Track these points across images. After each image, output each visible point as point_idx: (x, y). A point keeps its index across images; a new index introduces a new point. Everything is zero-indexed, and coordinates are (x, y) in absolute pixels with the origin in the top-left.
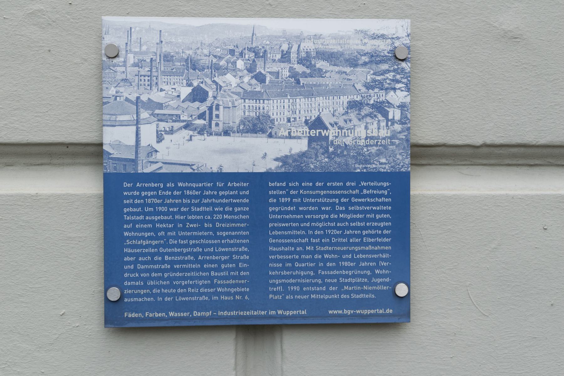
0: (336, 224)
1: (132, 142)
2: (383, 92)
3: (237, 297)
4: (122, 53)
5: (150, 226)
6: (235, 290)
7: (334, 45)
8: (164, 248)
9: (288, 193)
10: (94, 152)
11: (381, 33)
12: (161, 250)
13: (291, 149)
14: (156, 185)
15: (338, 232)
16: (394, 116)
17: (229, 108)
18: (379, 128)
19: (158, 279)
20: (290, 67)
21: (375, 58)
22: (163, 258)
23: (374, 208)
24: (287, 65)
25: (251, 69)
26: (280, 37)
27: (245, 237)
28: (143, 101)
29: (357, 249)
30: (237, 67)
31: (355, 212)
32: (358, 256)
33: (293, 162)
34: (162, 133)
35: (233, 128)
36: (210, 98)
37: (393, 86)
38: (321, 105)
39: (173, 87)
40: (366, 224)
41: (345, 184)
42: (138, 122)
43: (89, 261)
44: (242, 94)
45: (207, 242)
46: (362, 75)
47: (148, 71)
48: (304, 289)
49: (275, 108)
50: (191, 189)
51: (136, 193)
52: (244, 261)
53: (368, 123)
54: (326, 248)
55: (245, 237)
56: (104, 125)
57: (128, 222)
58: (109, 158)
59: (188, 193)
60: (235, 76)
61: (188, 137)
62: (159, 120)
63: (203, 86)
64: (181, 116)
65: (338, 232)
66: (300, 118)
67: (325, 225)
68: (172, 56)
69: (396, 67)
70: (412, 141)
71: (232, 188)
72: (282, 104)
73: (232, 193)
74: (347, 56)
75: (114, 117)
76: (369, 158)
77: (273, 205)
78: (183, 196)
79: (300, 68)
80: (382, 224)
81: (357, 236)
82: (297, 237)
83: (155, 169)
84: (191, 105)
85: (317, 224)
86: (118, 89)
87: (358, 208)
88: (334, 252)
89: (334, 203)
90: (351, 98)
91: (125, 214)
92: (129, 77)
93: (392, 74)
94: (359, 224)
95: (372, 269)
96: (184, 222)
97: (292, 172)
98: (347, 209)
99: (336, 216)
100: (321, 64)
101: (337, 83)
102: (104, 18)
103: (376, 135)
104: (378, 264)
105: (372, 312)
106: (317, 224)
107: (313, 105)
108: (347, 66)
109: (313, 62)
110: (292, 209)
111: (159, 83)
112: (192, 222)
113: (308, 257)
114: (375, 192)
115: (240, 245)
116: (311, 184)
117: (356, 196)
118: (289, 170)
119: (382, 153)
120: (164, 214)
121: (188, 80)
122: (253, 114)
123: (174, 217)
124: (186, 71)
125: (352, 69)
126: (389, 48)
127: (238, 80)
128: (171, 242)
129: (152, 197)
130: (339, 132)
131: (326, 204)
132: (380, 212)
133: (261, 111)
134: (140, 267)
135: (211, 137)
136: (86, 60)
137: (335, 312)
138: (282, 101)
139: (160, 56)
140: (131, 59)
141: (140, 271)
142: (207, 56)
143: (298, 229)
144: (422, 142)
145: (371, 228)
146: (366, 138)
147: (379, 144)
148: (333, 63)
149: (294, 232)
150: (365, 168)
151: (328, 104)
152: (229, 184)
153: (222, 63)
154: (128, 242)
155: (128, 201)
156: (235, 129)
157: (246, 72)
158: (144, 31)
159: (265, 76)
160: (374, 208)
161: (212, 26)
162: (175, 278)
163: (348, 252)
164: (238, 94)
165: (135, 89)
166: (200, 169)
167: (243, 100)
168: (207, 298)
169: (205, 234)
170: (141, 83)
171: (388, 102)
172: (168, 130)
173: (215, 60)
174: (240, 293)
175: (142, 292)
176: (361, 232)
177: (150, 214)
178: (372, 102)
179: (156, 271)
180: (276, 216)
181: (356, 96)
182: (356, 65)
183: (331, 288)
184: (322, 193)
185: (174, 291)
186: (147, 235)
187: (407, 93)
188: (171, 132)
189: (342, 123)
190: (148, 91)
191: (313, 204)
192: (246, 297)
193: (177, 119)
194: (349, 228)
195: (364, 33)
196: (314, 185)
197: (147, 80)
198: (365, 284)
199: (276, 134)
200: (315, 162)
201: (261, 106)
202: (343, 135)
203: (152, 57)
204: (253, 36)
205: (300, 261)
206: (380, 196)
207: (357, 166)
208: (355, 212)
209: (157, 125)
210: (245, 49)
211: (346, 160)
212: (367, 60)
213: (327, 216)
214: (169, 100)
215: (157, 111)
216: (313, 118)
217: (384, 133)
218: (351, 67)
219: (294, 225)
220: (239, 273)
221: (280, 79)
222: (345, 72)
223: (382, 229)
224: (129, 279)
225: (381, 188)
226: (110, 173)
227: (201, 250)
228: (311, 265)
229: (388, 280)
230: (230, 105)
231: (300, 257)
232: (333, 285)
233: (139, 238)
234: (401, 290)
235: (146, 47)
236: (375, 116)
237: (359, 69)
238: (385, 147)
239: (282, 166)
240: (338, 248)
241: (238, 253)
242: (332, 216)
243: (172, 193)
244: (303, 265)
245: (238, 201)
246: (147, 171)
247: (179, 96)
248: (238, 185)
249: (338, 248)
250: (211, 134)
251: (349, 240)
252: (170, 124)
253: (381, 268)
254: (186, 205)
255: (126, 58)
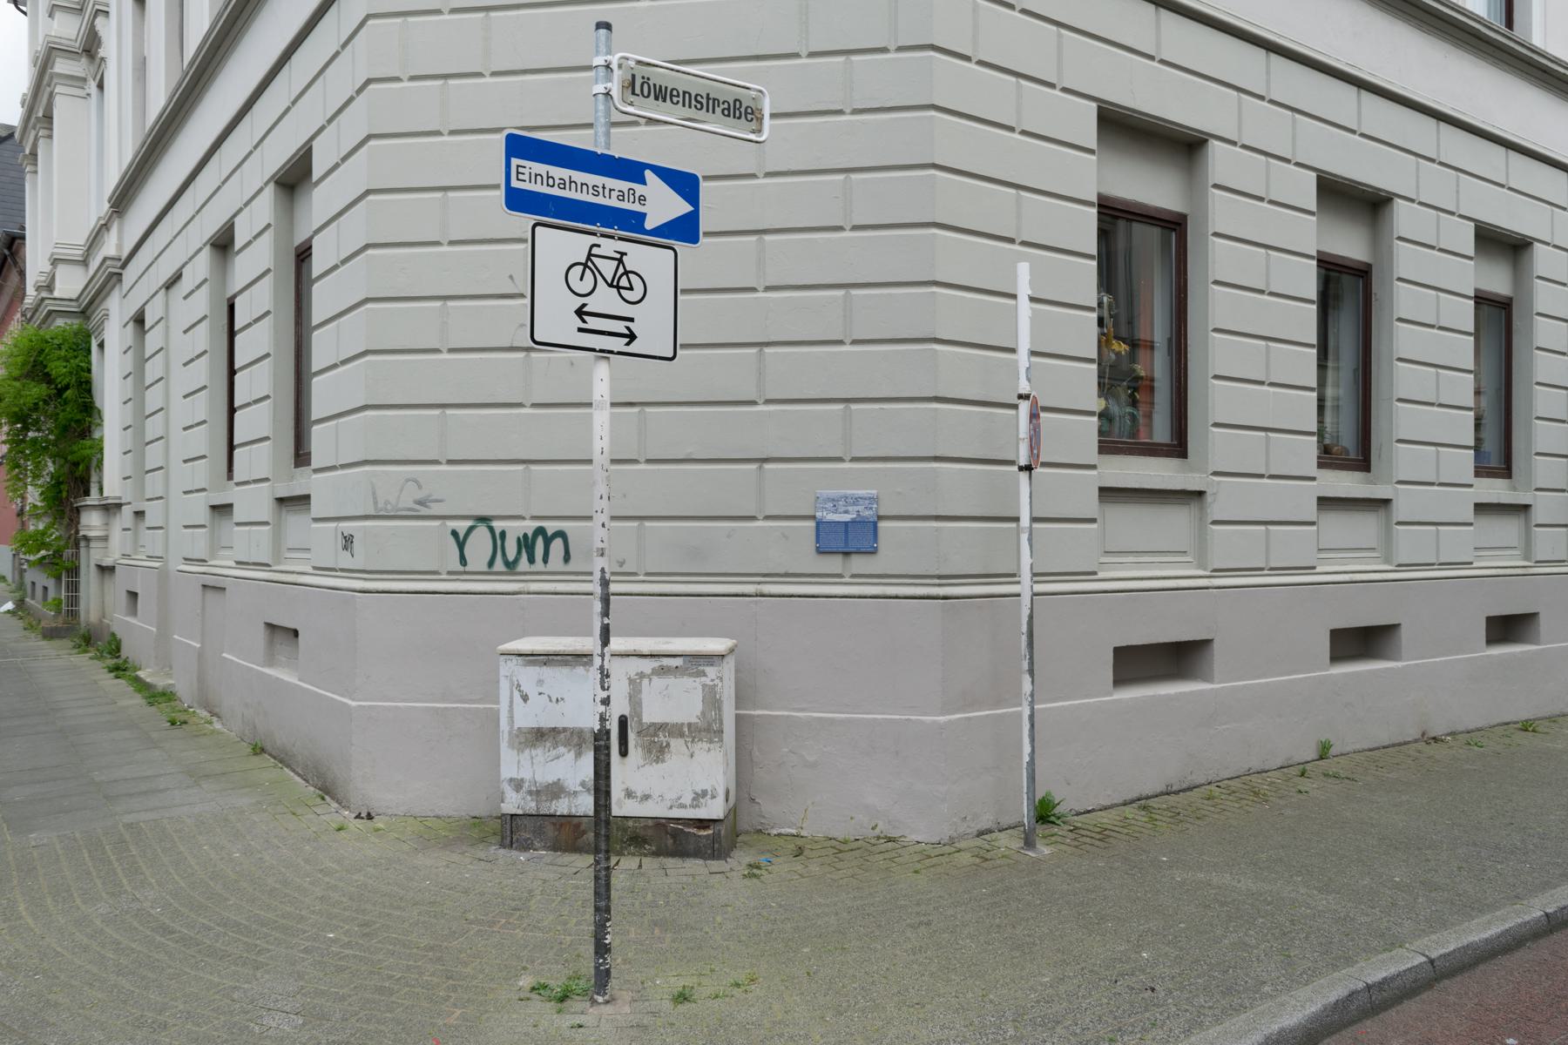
10: (814, 517)
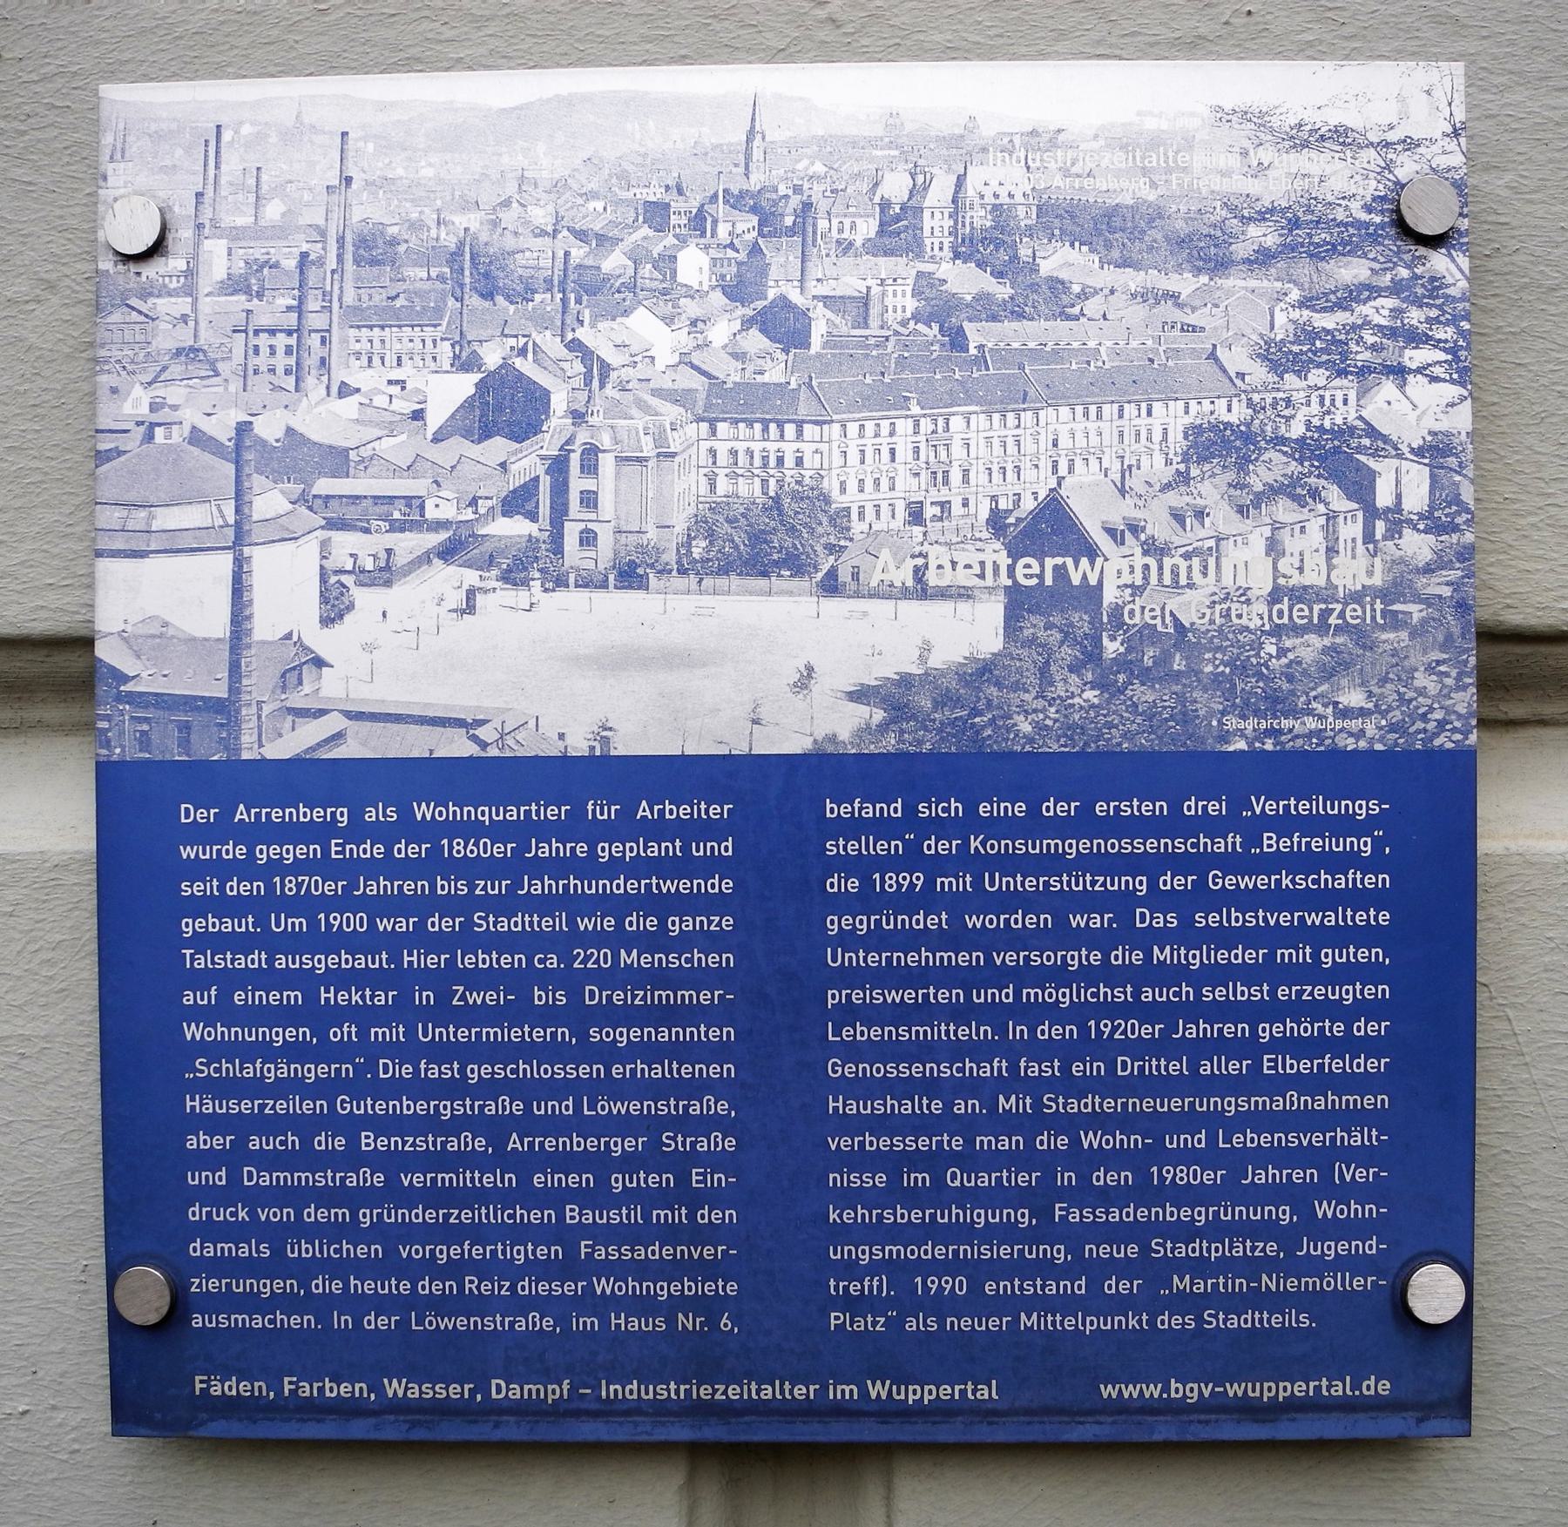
0: (1137, 994)
1: (217, 624)
2: (1349, 385)
3: (686, 1322)
4: (182, 235)
5: (294, 996)
6: (675, 1287)
7: (1118, 174)
8: (357, 1097)
9: (914, 849)
11: (1333, 122)
12: (345, 1106)
13: (926, 649)
14: (317, 814)
15: (1145, 1031)
16: (1399, 496)
17: (641, 460)
18: (1331, 551)
19: (335, 1232)
20: (920, 274)
21: (1306, 233)
22: (353, 1142)
23: (1313, 919)
24: (905, 268)
25: (738, 288)
26: (873, 142)
27: (718, 1052)
28: (264, 443)
29: (1231, 1106)
30: (682, 277)
31: (1225, 938)
32: (1237, 1139)
33: (938, 705)
34: (345, 579)
35: (659, 551)
36: (557, 421)
37: (1391, 358)
38: (1065, 442)
39: (396, 374)
40: (1273, 993)
41: (1175, 807)
42: (240, 537)
43: (63, 1139)
44: (702, 396)
45: (546, 1071)
46: (1250, 310)
47: (289, 309)
48: (990, 1287)
49: (853, 457)
50: (472, 830)
51: (234, 851)
52: (715, 1161)
53: (1283, 525)
54: (1091, 1103)
55: (718, 1052)
56: (99, 554)
57: (200, 980)
58: (121, 698)
59: (459, 848)
60: (668, 320)
61: (457, 598)
62: (332, 525)
63: (525, 366)
64: (429, 504)
65: (1145, 1031)
66: (965, 504)
67: (1088, 995)
68: (394, 242)
69: (1404, 273)
70: (1484, 614)
71: (657, 830)
72: (884, 440)
73: (654, 851)
74: (1180, 224)
75: (143, 514)
76: (1286, 686)
77: (843, 905)
78: (435, 865)
79: (965, 280)
80: (1348, 994)
81: (1233, 1048)
82: (957, 1051)
83: (312, 742)
84: (474, 451)
85: (1049, 995)
86: (159, 391)
87: (1236, 918)
88: (1126, 1122)
89: (1129, 896)
90: (1200, 411)
91: (188, 943)
92: (206, 337)
93: (1389, 303)
94: (1242, 993)
95: (1299, 1197)
96: (442, 981)
97: (930, 754)
98: (1187, 922)
99: (1137, 957)
100: (1060, 260)
101: (1134, 344)
102: (114, 92)
103: (1322, 582)
104: (1327, 1173)
105: (1299, 1389)
106: (1049, 995)
107: (1028, 446)
108: (1179, 269)
109: (1024, 252)
110: (932, 922)
111: (334, 361)
112: (476, 980)
113: (1005, 1144)
114: (1316, 844)
115: (695, 1089)
116: (1020, 809)
117: (1229, 863)
118: (920, 742)
119: (1347, 666)
120: (352, 942)
121: (460, 342)
122: (749, 489)
123: (395, 958)
124: (451, 302)
125: (1204, 279)
126: (1372, 188)
127: (683, 339)
128: (388, 1069)
129: (299, 867)
130: (1146, 567)
131: (1089, 902)
132: (1341, 937)
133: (790, 473)
134: (253, 1177)
135: (560, 596)
136: (51, 287)
137: (1130, 1391)
138: (885, 430)
139: (341, 241)
140: (218, 260)
141: (256, 1197)
142: (544, 233)
143: (960, 1014)
144: (1515, 618)
145: (1297, 1009)
146: (1274, 597)
147: (1333, 620)
148: (1116, 254)
149: (943, 1031)
150: (1273, 733)
151: (1094, 440)
152: (644, 810)
153: (614, 262)
154: (204, 1069)
155: (198, 888)
156: (670, 557)
157: (718, 298)
158: (273, 139)
159: (804, 315)
160: (1313, 919)
161: (569, 103)
162: (409, 1233)
163: (1189, 1121)
164: (679, 398)
165: (232, 388)
166: (510, 741)
167: (704, 426)
168: (548, 1323)
169: (538, 1034)
170: (257, 361)
171: (1372, 432)
172: (369, 566)
173: (578, 253)
174: (697, 1304)
175: (266, 1288)
176: (1254, 1031)
177: (293, 944)
178: (1297, 430)
179: (326, 1197)
180: (856, 958)
181: (1223, 402)
182: (1220, 265)
183: (1111, 1286)
184: (1074, 848)
185: (405, 1287)
186: (280, 1036)
187: (1454, 391)
188: (384, 574)
189: (1159, 527)
190: (284, 398)
191: (1027, 902)
192: (725, 1322)
193: (410, 515)
194: (1195, 1011)
195: (1256, 119)
196: (1034, 810)
197: (280, 351)
198: (1269, 1265)
199: (855, 576)
200: (1040, 704)
201: (789, 449)
202: (1167, 580)
203: (305, 247)
204: (749, 140)
205: (969, 1160)
206: (1338, 863)
207: (1232, 723)
208: (1225, 938)
209: (325, 544)
210: (715, 196)
211: (1181, 698)
212: (1271, 241)
213: (1096, 957)
214: (378, 433)
215: (324, 486)
216: (1029, 504)
217: (1354, 571)
218: (1198, 271)
219: (943, 996)
220: (691, 1216)
221: (874, 329)
222: (1174, 297)
223: (1348, 1014)
224: (211, 1232)
225: (1346, 825)
226: (122, 763)
227: (518, 1107)
228: (1022, 1179)
229: (1371, 1247)
230: (648, 449)
231: (970, 1142)
232: (1124, 1269)
233: (247, 1052)
234: (1435, 1294)
235: (283, 208)
236: (1315, 494)
237: (1235, 282)
238: (1360, 634)
239: (883, 727)
240: (1147, 1105)
241: (683, 1124)
242: (1118, 957)
243: (389, 852)
244: (985, 1180)
245: (683, 885)
246: (280, 749)
247: (418, 415)
248: (684, 811)
249: (1147, 1105)
250: (561, 582)
251: (1194, 1067)
252: (379, 541)
253: (1342, 1194)
254: (448, 906)
255: (196, 256)
